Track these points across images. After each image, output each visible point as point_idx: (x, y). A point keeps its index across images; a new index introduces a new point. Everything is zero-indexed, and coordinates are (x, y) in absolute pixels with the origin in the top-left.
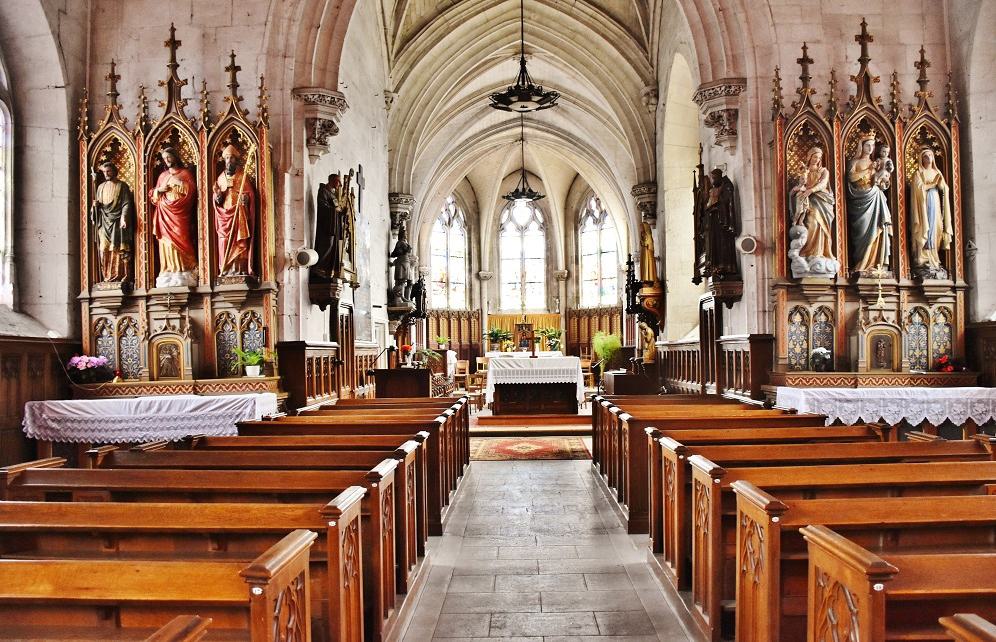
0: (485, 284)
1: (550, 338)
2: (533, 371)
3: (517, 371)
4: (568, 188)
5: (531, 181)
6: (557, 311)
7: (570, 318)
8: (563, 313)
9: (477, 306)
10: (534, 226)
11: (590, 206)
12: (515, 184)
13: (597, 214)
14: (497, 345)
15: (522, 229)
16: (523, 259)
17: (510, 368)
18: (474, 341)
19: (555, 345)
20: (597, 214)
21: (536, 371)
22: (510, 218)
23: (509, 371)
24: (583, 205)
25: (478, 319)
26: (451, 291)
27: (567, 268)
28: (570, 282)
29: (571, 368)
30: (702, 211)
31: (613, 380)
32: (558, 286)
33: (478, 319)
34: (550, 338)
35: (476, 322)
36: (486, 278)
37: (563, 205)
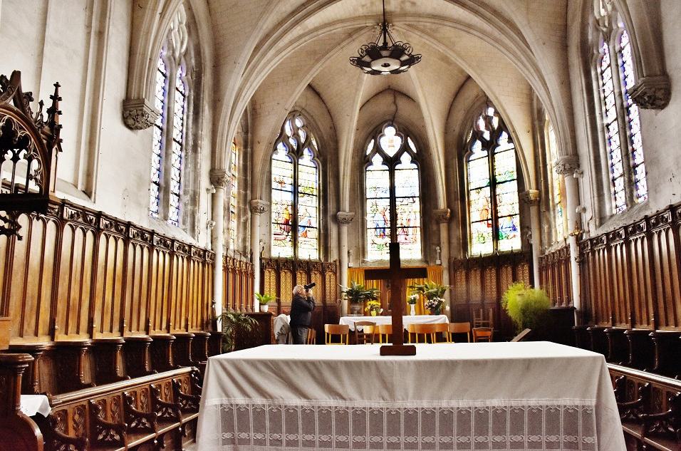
0: (345, 229)
1: (430, 296)
2: (394, 417)
3: (325, 414)
4: (448, 107)
5: (402, 103)
6: (438, 262)
7: (455, 271)
8: (445, 265)
9: (334, 257)
10: (406, 158)
11: (478, 127)
12: (385, 105)
13: (487, 136)
14: (357, 307)
15: (392, 163)
16: (393, 198)
17: (259, 400)
18: (330, 299)
19: (437, 306)
20: (487, 136)
21: (411, 416)
22: (377, 149)
23: (291, 413)
24: (468, 127)
25: (335, 274)
26: (300, 239)
27: (449, 206)
28: (454, 225)
29: (568, 401)
30: (665, 89)
31: (453, 324)
32: (439, 231)
33: (335, 274)
34: (430, 296)
35: (333, 277)
36: (346, 221)
37: (442, 130)
